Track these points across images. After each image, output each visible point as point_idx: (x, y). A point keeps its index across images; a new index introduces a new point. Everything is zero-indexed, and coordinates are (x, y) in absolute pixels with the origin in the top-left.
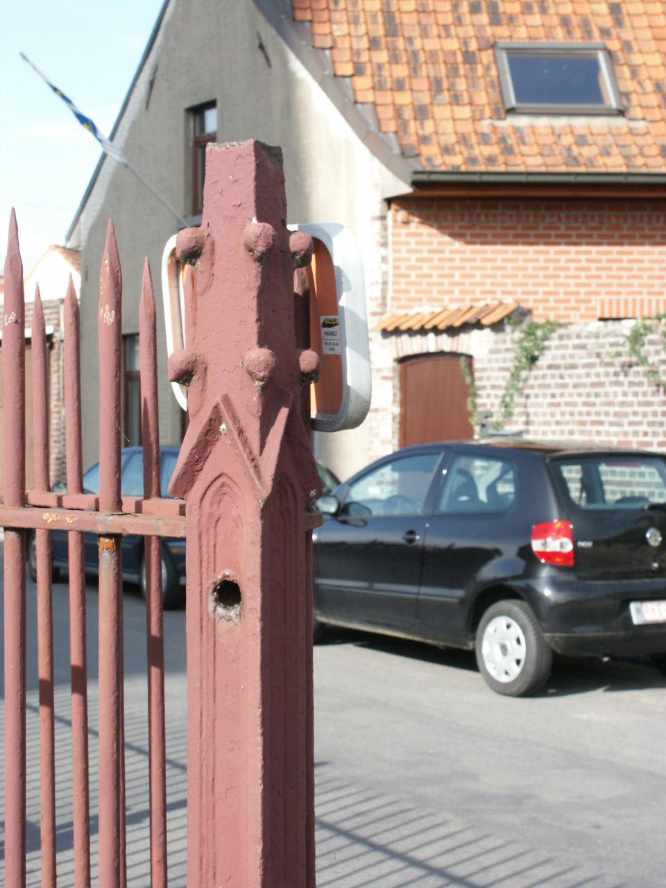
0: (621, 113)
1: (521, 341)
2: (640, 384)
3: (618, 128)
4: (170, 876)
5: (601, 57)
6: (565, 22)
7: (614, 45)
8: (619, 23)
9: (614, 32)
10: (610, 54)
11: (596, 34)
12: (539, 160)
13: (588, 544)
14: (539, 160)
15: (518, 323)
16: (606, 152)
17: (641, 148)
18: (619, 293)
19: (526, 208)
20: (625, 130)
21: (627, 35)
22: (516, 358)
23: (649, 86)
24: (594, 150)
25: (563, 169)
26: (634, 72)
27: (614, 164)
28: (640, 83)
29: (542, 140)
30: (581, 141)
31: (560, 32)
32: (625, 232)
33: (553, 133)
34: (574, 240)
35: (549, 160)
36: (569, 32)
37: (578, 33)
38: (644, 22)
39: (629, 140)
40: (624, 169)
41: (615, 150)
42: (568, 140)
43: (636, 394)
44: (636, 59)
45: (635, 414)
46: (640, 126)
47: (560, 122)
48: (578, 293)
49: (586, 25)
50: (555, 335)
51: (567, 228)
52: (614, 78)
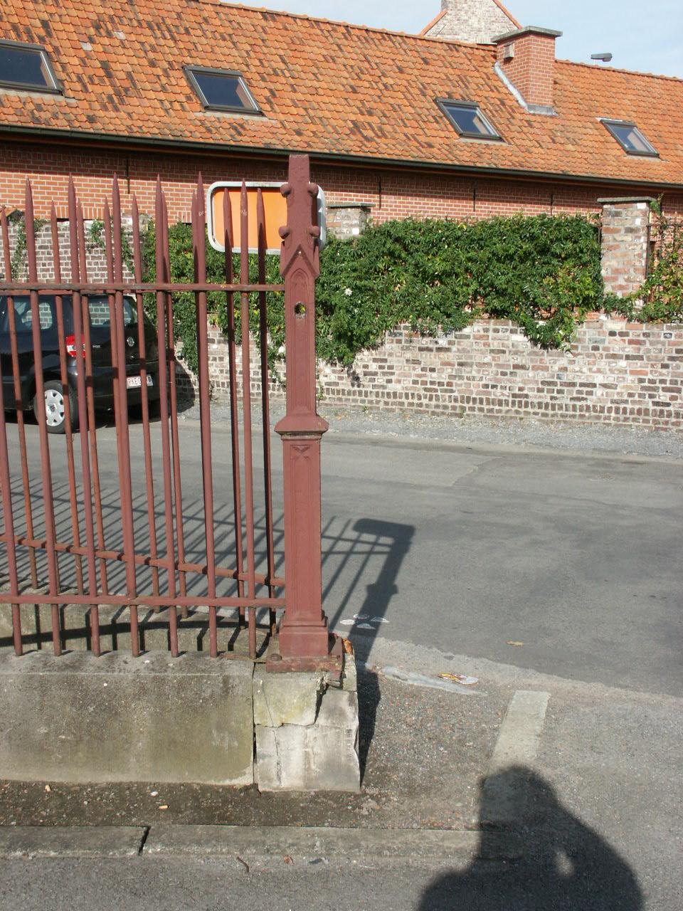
0: (60, 93)
1: (21, 231)
2: (99, 258)
3: (59, 102)
4: (56, 513)
5: (42, 55)
6: (15, 28)
7: (49, 49)
8: (49, 34)
9: (47, 39)
10: (47, 54)
11: (37, 40)
12: (16, 118)
13: (99, 346)
14: (16, 118)
15: (16, 221)
16: (55, 117)
17: (76, 115)
18: (93, 205)
19: (9, 148)
20: (64, 104)
21: (57, 43)
22: (19, 242)
23: (75, 79)
24: (49, 115)
25: (32, 125)
26: (63, 66)
27: (61, 124)
28: (67, 75)
29: (15, 105)
30: (39, 107)
31: (13, 34)
32: (32, 164)
33: (20, 101)
34: (39, 170)
35: (22, 119)
36: (19, 36)
37: (25, 37)
38: (64, 36)
39: (68, 110)
40: (126, 134)
41: (61, 116)
42: (31, 107)
43: (97, 264)
44: (64, 59)
45: (97, 275)
46: (73, 101)
47: (24, 95)
48: (44, 203)
49: (28, 32)
50: (43, 228)
51: (34, 162)
52: (53, 70)
